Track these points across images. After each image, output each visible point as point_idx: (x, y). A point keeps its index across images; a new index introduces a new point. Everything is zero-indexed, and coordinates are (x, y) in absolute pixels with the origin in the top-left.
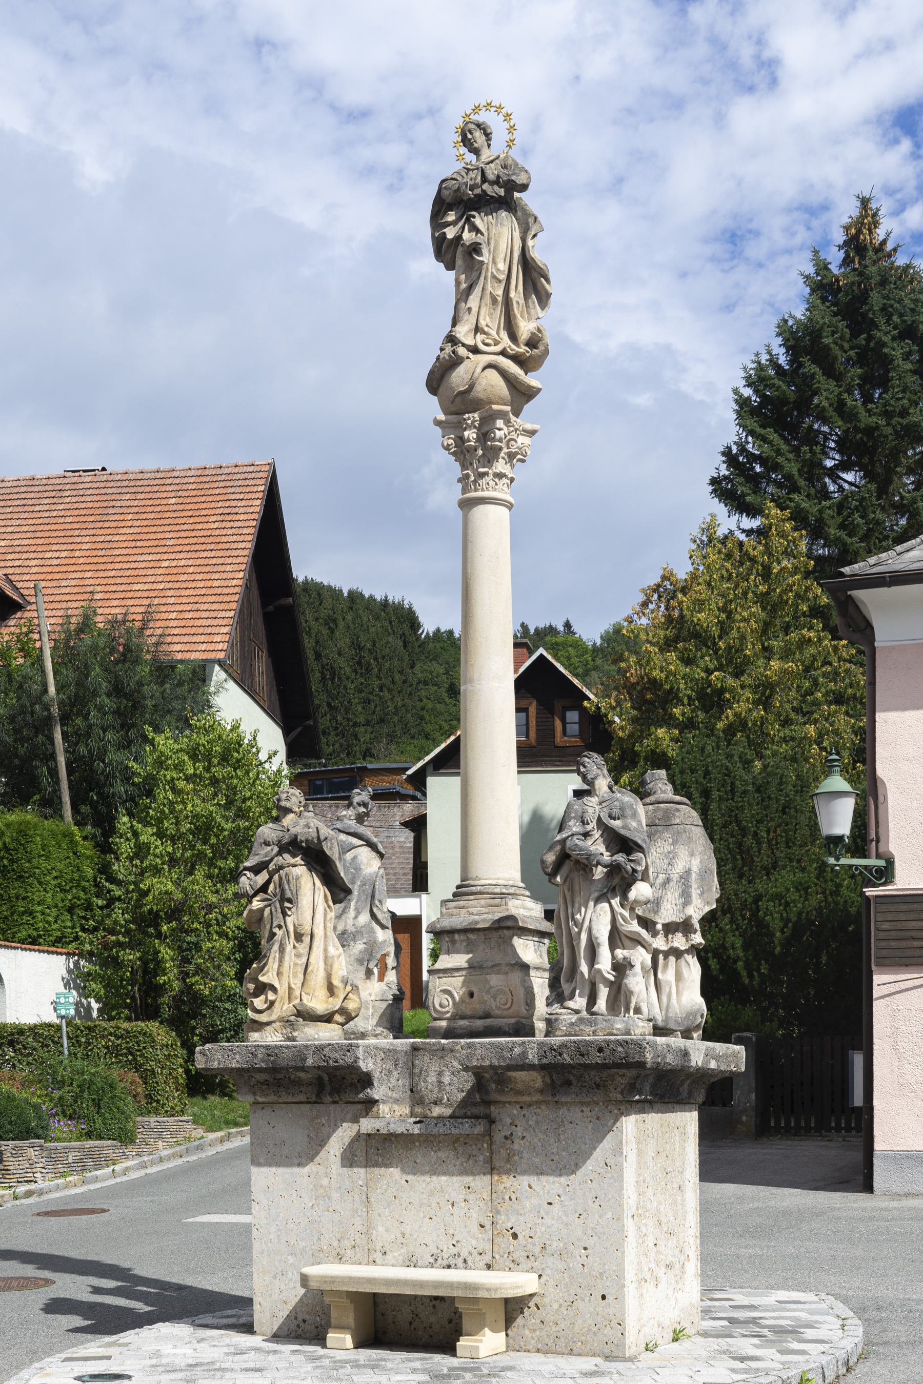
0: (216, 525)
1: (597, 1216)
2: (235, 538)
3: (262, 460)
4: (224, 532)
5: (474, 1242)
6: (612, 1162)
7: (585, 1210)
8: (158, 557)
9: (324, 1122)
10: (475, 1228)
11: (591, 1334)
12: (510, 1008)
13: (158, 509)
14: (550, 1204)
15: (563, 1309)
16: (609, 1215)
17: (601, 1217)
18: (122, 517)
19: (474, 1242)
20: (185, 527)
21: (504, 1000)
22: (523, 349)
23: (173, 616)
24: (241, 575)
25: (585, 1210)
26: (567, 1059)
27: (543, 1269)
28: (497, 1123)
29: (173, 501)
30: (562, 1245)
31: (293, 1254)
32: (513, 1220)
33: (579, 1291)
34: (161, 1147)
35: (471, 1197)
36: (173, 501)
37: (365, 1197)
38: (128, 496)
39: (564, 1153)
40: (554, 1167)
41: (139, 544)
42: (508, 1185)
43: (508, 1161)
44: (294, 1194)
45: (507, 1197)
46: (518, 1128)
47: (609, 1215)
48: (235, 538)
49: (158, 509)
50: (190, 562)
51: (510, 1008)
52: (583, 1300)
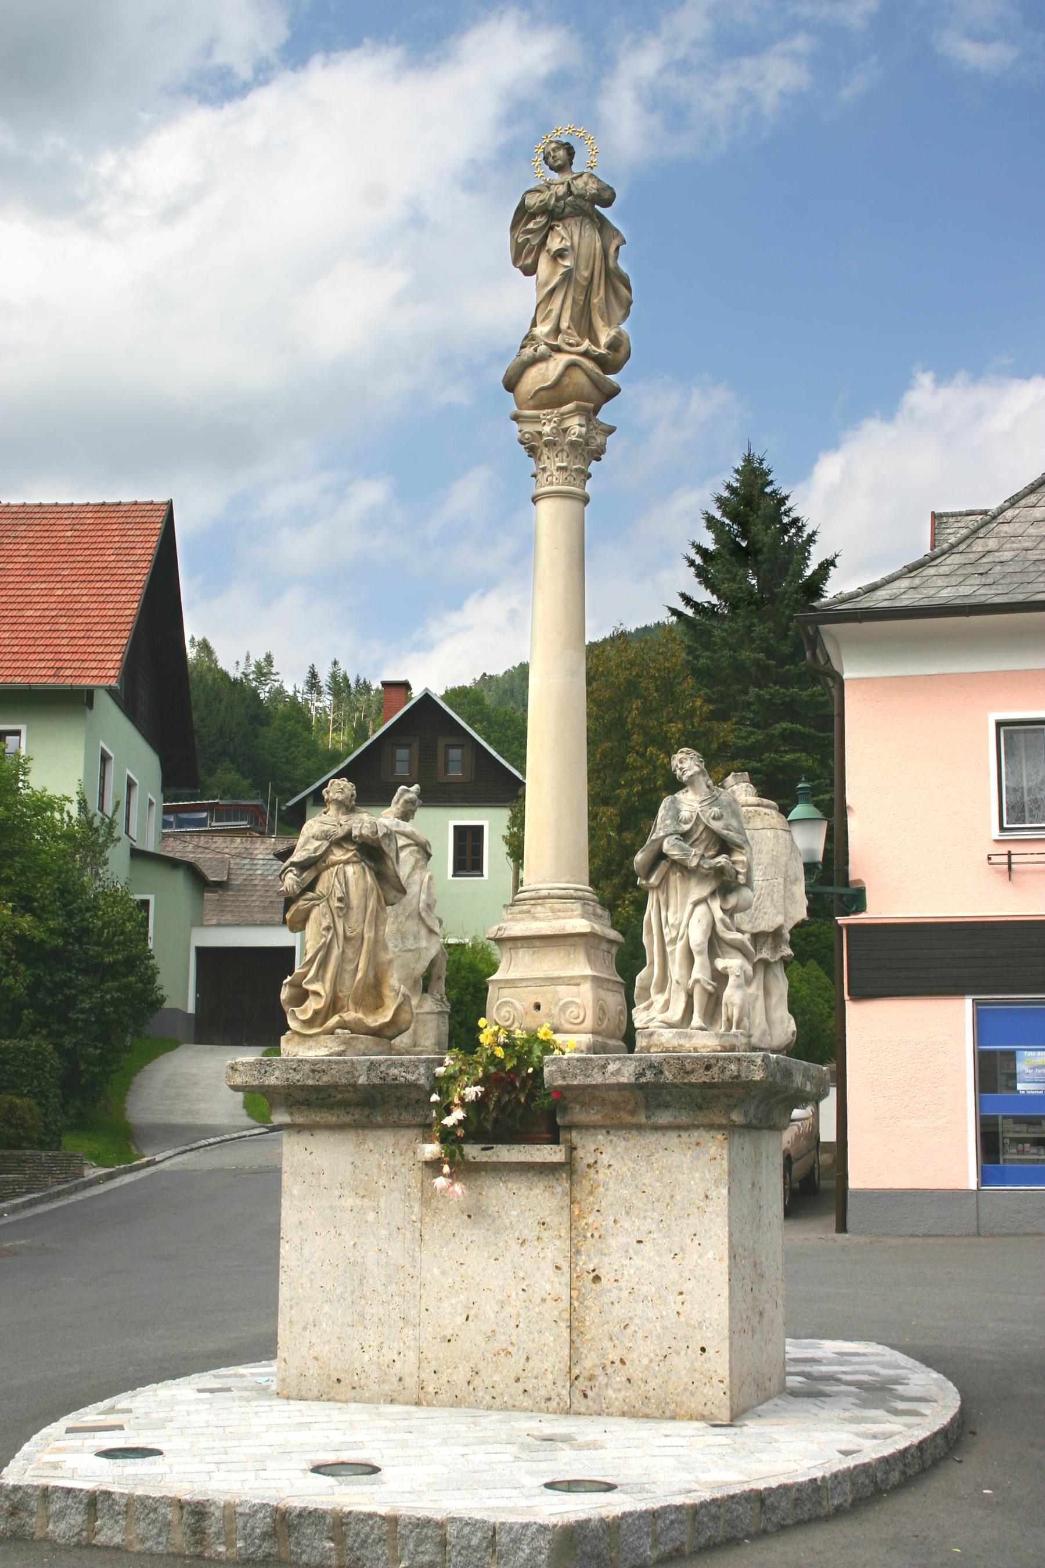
0: (112, 558)
1: (695, 1256)
2: (131, 571)
3: (160, 498)
4: (120, 565)
5: (548, 1287)
6: (714, 1194)
7: (682, 1249)
8: (52, 585)
9: (372, 1147)
10: (550, 1271)
11: (687, 1393)
12: (583, 1022)
13: (54, 540)
14: (640, 1242)
15: (654, 1364)
16: (710, 1255)
17: (700, 1257)
18: (16, 547)
19: (548, 1287)
20: (80, 559)
21: (575, 1014)
22: (603, 351)
23: (64, 642)
24: (135, 605)
25: (682, 1249)
26: (668, 1076)
27: (631, 1318)
28: (579, 1150)
29: (69, 534)
30: (653, 1290)
31: (329, 1301)
32: (596, 1261)
33: (673, 1343)
34: (50, 1184)
35: (545, 1235)
36: (69, 534)
37: (418, 1234)
38: (24, 528)
39: (658, 1184)
40: (645, 1200)
41: (33, 572)
42: (590, 1221)
43: (591, 1193)
44: (333, 1231)
45: (589, 1235)
46: (604, 1156)
47: (710, 1255)
48: (131, 571)
49: (54, 540)
50: (85, 592)
51: (583, 1022)
52: (678, 1354)
